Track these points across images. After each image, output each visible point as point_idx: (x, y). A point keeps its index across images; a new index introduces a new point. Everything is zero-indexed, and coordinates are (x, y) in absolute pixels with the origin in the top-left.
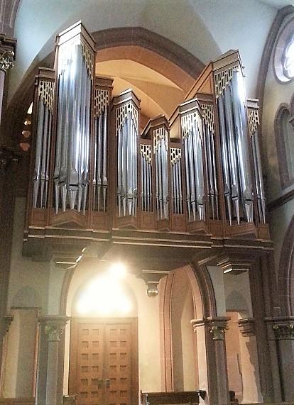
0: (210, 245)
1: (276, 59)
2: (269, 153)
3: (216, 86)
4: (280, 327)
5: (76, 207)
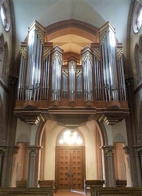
0: (95, 112)
1: (133, 24)
2: (133, 67)
3: (101, 39)
5: (32, 99)
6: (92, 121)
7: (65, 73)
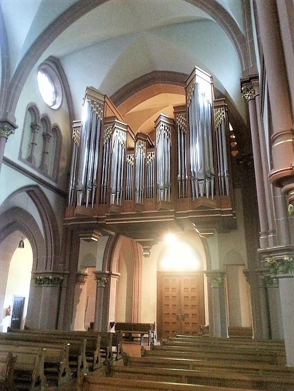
4: (55, 279)
6: (17, 231)
7: (130, 160)
